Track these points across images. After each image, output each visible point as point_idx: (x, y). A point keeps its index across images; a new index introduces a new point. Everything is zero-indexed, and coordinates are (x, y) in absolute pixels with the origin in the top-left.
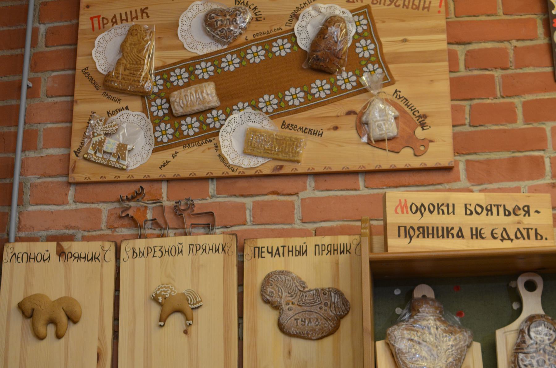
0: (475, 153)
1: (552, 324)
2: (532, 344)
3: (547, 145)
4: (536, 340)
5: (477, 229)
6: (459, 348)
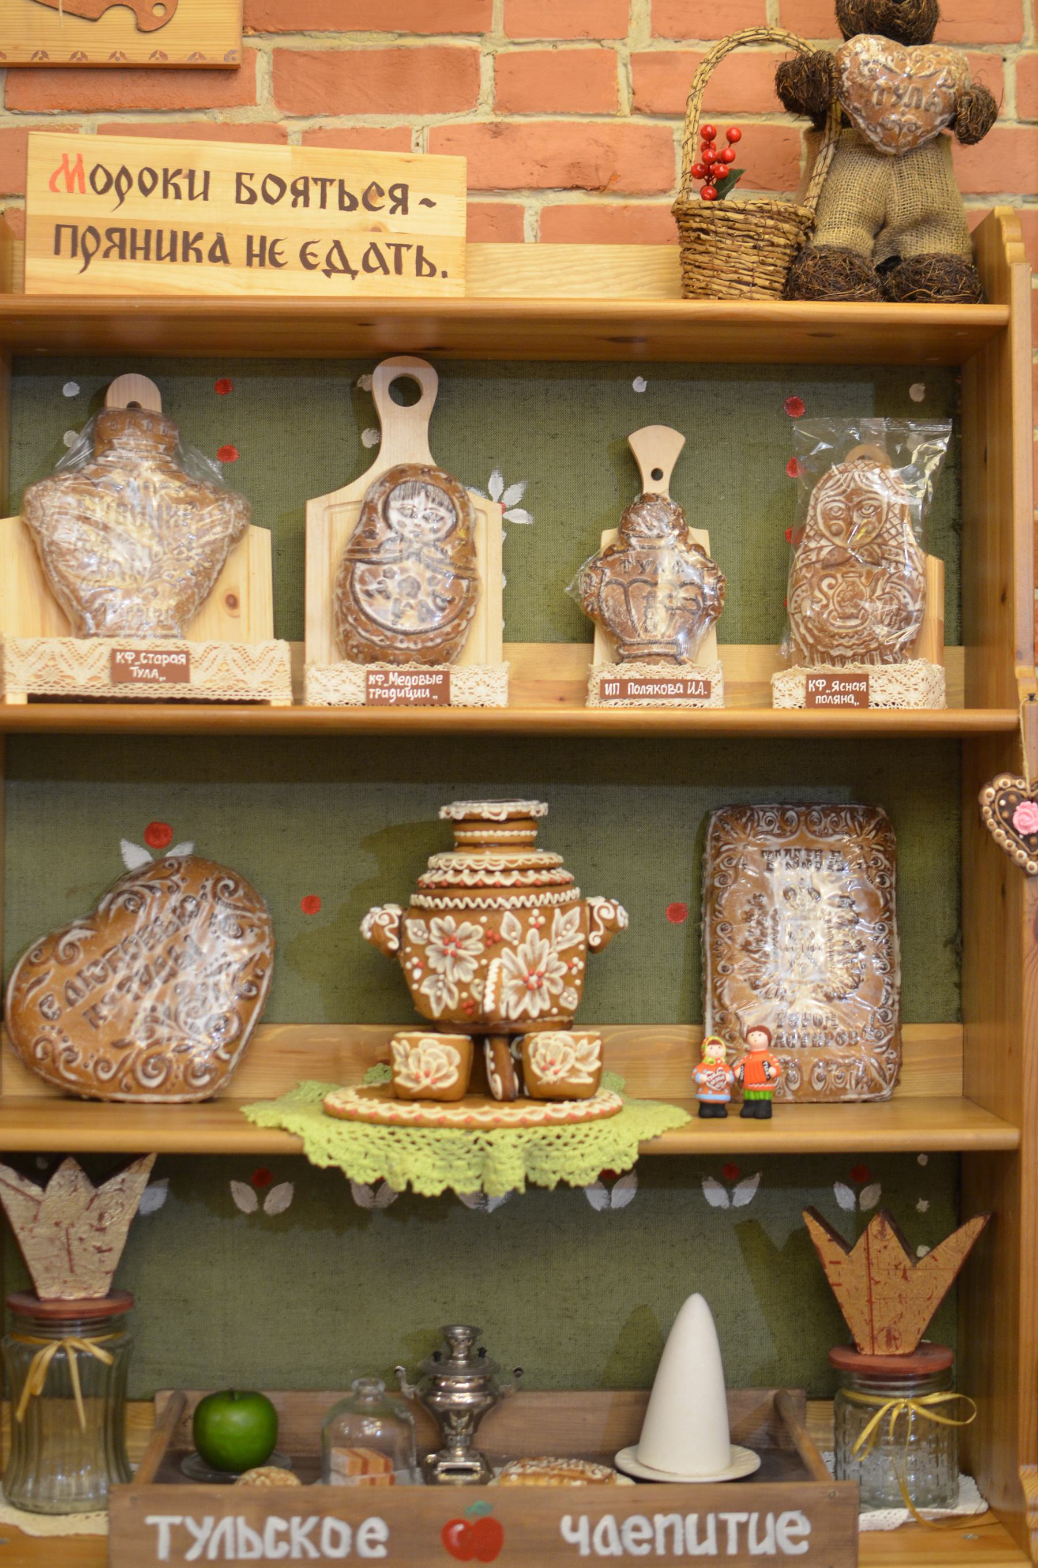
0: (301, 32)
1: (445, 492)
3: (490, 24)
5: (263, 239)
6: (209, 543)
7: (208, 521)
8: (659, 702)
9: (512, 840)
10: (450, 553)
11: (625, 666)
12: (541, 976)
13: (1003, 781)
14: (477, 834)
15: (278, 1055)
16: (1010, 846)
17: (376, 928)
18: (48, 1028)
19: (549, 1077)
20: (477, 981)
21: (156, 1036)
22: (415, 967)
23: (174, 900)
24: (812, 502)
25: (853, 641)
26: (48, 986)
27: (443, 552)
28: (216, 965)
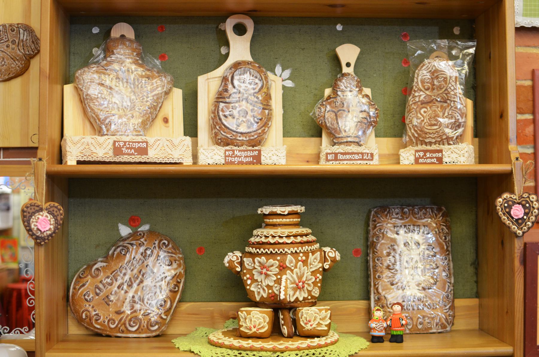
1: (258, 72)
2: (234, 93)
4: (239, 89)
6: (156, 95)
7: (155, 85)
8: (352, 162)
9: (290, 223)
10: (260, 98)
11: (336, 147)
12: (303, 283)
13: (506, 195)
14: (275, 220)
15: (187, 316)
16: (509, 224)
17: (230, 262)
18: (87, 306)
19: (308, 327)
20: (276, 285)
21: (134, 309)
22: (248, 279)
23: (142, 249)
24: (416, 76)
25: (435, 135)
26: (87, 287)
27: (257, 98)
28: (160, 277)
